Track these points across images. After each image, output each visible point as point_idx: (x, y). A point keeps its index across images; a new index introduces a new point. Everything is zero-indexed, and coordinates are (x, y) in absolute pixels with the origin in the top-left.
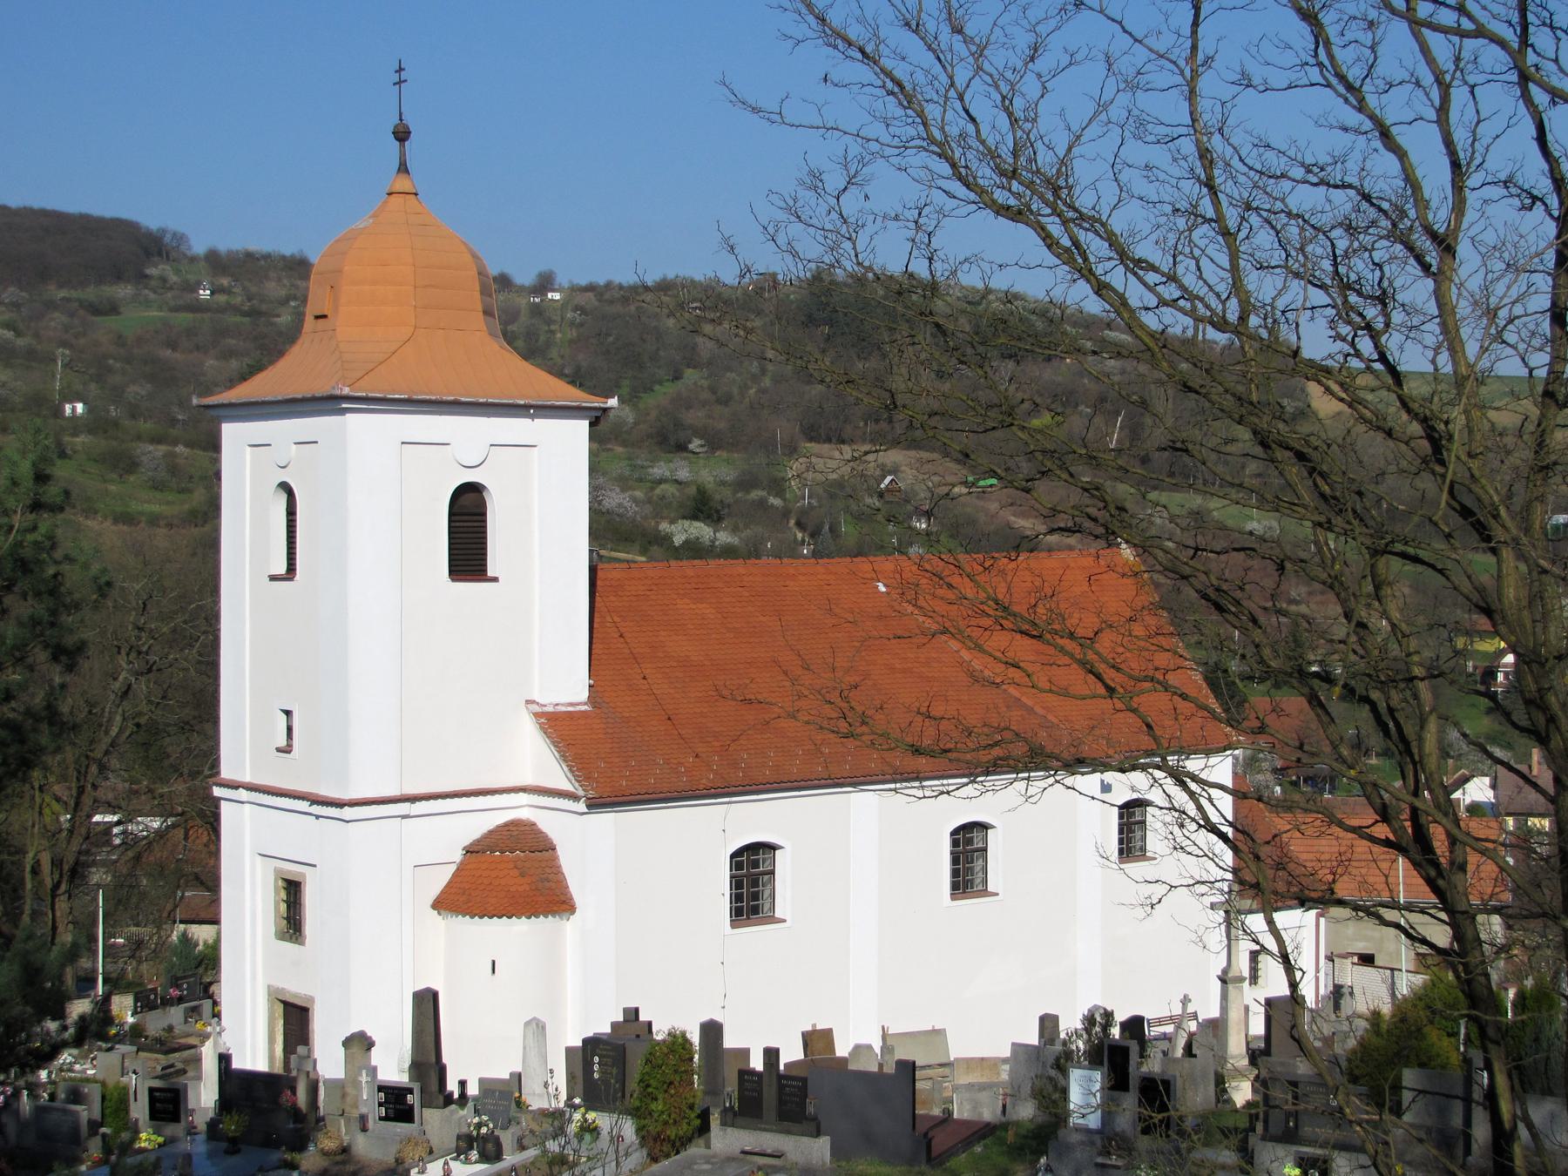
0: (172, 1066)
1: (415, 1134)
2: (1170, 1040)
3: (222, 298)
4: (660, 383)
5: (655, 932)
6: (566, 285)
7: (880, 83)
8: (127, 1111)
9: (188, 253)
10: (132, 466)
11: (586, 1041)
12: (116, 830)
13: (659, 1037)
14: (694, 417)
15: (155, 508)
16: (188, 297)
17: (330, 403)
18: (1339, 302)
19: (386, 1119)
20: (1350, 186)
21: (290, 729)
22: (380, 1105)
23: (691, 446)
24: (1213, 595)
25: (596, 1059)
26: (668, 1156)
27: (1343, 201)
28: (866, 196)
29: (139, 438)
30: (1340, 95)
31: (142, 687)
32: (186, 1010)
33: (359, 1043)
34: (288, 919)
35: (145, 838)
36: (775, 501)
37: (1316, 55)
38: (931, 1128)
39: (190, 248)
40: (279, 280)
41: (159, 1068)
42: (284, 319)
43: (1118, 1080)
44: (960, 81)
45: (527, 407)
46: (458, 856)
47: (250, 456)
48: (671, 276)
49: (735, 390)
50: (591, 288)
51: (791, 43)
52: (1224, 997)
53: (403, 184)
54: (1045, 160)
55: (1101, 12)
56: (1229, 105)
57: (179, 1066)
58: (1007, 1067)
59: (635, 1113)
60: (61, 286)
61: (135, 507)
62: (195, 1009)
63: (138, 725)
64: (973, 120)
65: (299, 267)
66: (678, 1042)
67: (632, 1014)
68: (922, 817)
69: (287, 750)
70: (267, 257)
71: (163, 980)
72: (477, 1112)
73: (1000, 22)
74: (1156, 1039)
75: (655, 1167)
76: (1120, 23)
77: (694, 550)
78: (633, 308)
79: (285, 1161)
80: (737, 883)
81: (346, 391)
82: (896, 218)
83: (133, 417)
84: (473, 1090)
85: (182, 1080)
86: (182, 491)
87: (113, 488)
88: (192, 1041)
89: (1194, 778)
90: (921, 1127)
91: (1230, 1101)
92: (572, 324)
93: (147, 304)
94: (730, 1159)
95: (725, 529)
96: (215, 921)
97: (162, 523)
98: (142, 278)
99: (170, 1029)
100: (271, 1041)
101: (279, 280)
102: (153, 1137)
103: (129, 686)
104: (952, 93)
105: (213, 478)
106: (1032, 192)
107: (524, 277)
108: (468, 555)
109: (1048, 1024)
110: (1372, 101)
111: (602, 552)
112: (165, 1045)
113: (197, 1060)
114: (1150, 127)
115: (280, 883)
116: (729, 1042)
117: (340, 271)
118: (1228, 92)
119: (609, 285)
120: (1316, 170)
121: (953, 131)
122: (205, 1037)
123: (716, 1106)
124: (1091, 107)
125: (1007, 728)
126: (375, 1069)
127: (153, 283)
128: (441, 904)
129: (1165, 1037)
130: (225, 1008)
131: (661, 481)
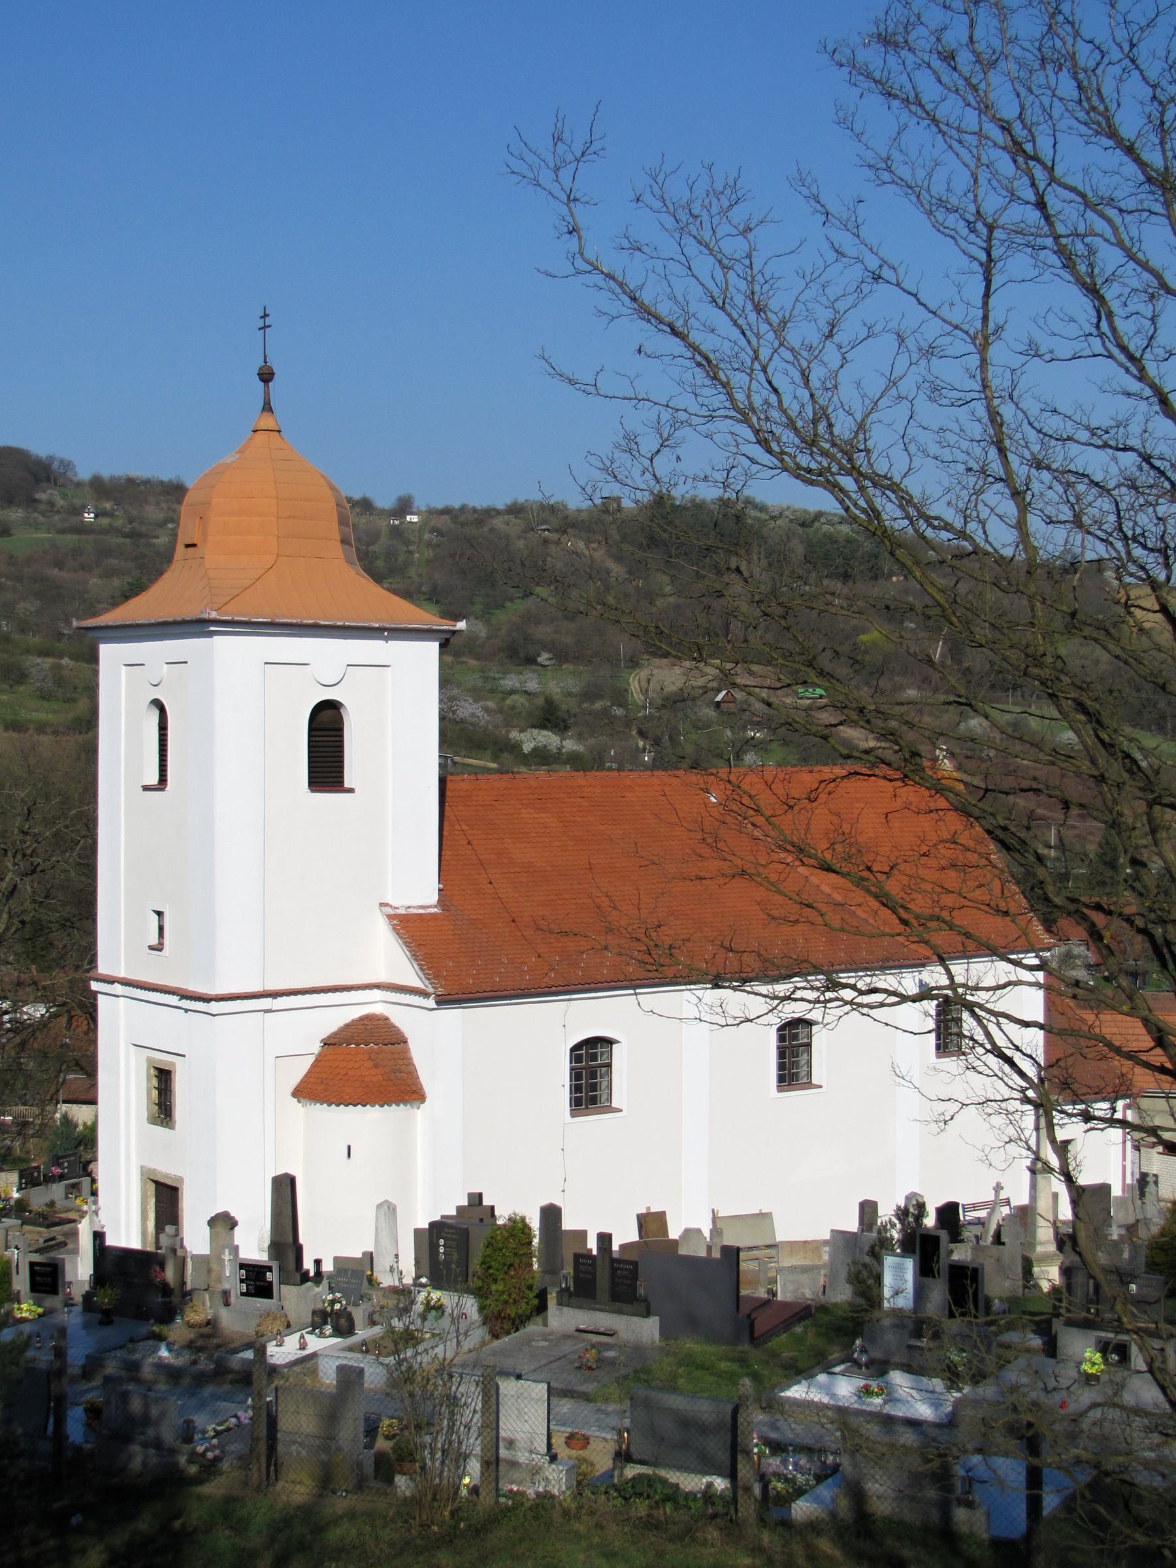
0: (53, 1239)
1: (273, 1308)
2: (983, 1224)
3: (105, 521)
4: (511, 600)
5: (498, 1123)
6: (424, 508)
7: (689, 355)
8: (10, 1283)
9: (75, 479)
10: (22, 677)
11: (433, 1225)
12: (6, 1017)
13: (500, 1222)
14: (543, 632)
15: (42, 716)
16: (74, 520)
17: (198, 627)
18: (1124, 555)
19: (246, 1294)
20: (1131, 449)
21: (161, 929)
22: (242, 1281)
23: (539, 659)
24: (998, 832)
25: (442, 1242)
26: (508, 1333)
27: (1129, 460)
28: (678, 459)
29: (28, 651)
30: (1121, 365)
31: (27, 887)
32: (67, 1186)
33: (223, 1223)
34: (159, 1105)
35: (30, 1025)
36: (618, 712)
37: (1098, 327)
38: (755, 1309)
39: (76, 474)
40: (158, 504)
41: (42, 1241)
42: (162, 540)
43: (925, 1270)
44: (764, 354)
45: (381, 630)
46: (316, 1048)
47: (126, 674)
48: (521, 500)
50: (447, 511)
51: (605, 319)
52: (1033, 1186)
53: (267, 422)
54: (843, 427)
55: (898, 285)
56: (1019, 372)
57: (60, 1238)
58: (827, 1249)
59: (480, 1293)
61: (24, 715)
62: (75, 1187)
63: (23, 922)
64: (776, 391)
65: (176, 491)
66: (518, 1227)
67: (476, 1199)
68: (746, 1019)
69: (158, 948)
70: (147, 482)
71: (45, 1159)
72: (331, 1290)
73: (801, 298)
74: (970, 1223)
75: (496, 1343)
76: (915, 296)
77: (542, 757)
78: (486, 529)
79: (154, 1332)
80: (576, 1074)
81: (214, 615)
82: (706, 479)
83: (23, 631)
84: (328, 1267)
85: (59, 1255)
86: (67, 701)
88: (72, 1215)
89: (981, 1007)
90: (745, 1309)
91: (1037, 1286)
92: (429, 544)
93: (37, 526)
94: (566, 1336)
95: (571, 738)
96: (93, 1102)
97: (49, 730)
98: (32, 502)
99: (52, 1204)
100: (144, 1217)
101: (158, 504)
102: (33, 1308)
103: (15, 886)
104: (757, 366)
105: (92, 690)
106: (832, 455)
107: (384, 501)
108: (326, 766)
109: (868, 1209)
110: (1151, 369)
111: (457, 759)
112: (48, 1219)
113: (75, 1234)
114: (944, 392)
115: (152, 1071)
116: (568, 1223)
117: (209, 503)
118: (1016, 361)
119: (463, 509)
120: (1099, 432)
121: (757, 401)
122: (83, 1214)
123: (553, 1285)
124: (882, 383)
125: (806, 961)
126: (237, 1248)
127: (42, 507)
128: (303, 1092)
129: (980, 1222)
130: (101, 1186)
131: (512, 692)
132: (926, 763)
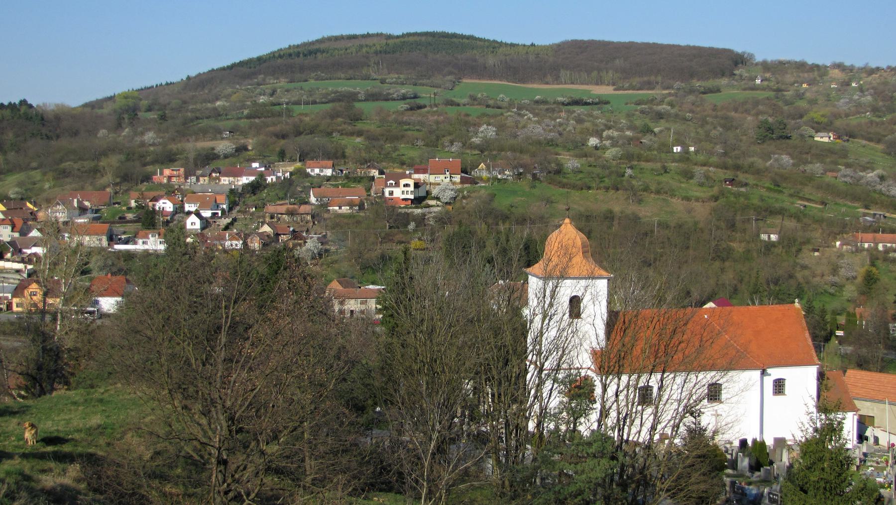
3: (766, 83)
15: (698, 194)
16: (751, 83)
70: (789, 62)
87: (683, 185)
93: (733, 87)
127: (736, 77)
132: (99, 322)
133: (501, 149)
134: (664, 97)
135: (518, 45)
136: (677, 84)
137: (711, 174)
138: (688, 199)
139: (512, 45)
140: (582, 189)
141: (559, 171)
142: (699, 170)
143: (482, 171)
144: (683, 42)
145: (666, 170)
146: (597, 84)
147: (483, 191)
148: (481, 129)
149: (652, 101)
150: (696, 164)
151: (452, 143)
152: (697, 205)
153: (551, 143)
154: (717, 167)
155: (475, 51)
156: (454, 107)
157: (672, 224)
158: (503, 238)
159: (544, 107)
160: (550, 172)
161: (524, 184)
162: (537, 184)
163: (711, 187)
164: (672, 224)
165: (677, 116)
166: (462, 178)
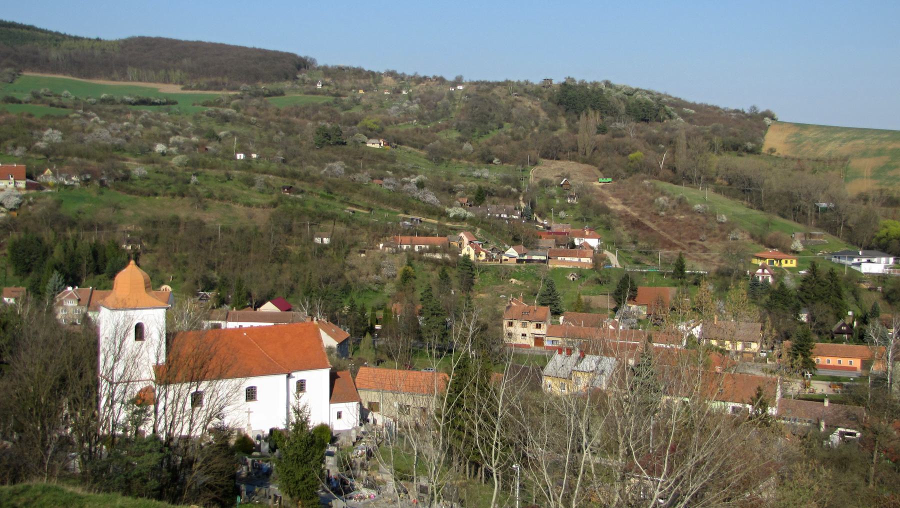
3: (326, 88)
15: (258, 201)
49: (521, 135)
60: (264, 82)
61: (252, 200)
70: (348, 68)
87: (245, 192)
92: (464, 101)
107: (450, 78)
127: (299, 81)
133: (67, 154)
134: (232, 98)
135: (82, 39)
136: (244, 86)
137: (270, 182)
138: (249, 205)
139: (76, 38)
140: (149, 195)
141: (127, 178)
142: (259, 178)
143: (48, 176)
144: (249, 44)
145: (229, 178)
146: (165, 82)
147: (49, 198)
148: (47, 133)
149: (218, 103)
150: (257, 172)
151: (15, 146)
152: (258, 212)
153: (119, 148)
154: (276, 174)
155: (36, 43)
156: (15, 105)
157: (235, 229)
158: (71, 243)
159: (111, 107)
160: (117, 179)
161: (92, 191)
162: (104, 190)
163: (271, 194)
164: (235, 229)
165: (242, 119)
166: (27, 184)
